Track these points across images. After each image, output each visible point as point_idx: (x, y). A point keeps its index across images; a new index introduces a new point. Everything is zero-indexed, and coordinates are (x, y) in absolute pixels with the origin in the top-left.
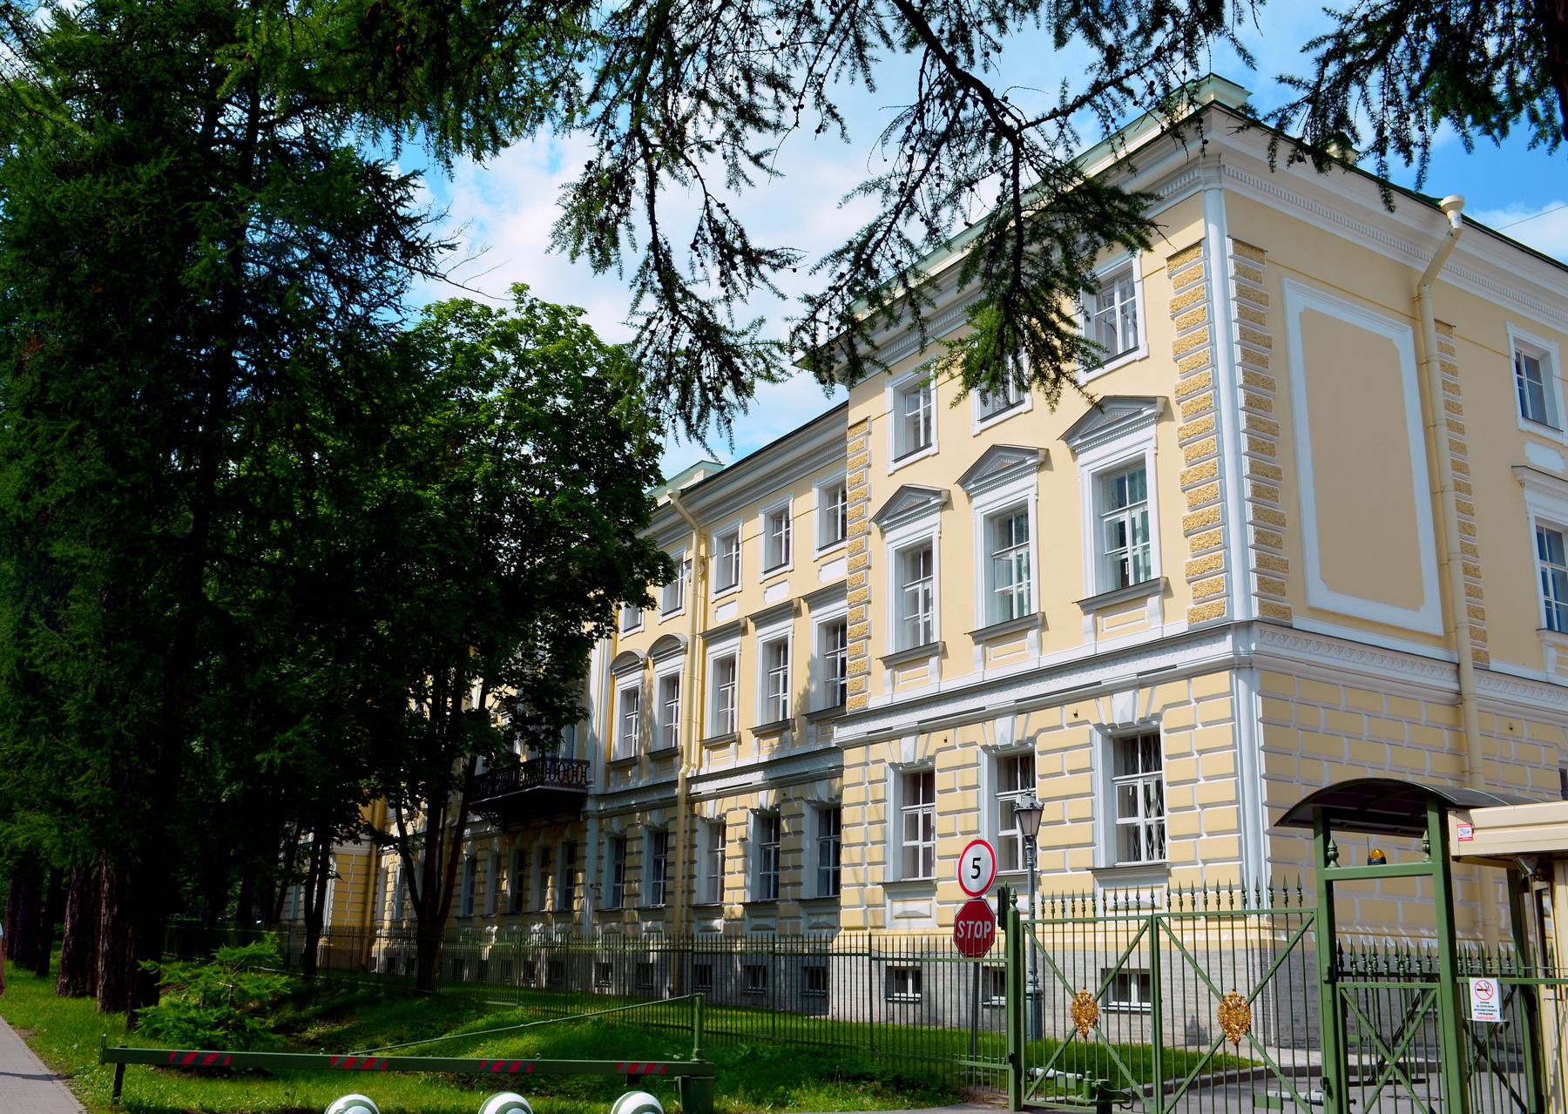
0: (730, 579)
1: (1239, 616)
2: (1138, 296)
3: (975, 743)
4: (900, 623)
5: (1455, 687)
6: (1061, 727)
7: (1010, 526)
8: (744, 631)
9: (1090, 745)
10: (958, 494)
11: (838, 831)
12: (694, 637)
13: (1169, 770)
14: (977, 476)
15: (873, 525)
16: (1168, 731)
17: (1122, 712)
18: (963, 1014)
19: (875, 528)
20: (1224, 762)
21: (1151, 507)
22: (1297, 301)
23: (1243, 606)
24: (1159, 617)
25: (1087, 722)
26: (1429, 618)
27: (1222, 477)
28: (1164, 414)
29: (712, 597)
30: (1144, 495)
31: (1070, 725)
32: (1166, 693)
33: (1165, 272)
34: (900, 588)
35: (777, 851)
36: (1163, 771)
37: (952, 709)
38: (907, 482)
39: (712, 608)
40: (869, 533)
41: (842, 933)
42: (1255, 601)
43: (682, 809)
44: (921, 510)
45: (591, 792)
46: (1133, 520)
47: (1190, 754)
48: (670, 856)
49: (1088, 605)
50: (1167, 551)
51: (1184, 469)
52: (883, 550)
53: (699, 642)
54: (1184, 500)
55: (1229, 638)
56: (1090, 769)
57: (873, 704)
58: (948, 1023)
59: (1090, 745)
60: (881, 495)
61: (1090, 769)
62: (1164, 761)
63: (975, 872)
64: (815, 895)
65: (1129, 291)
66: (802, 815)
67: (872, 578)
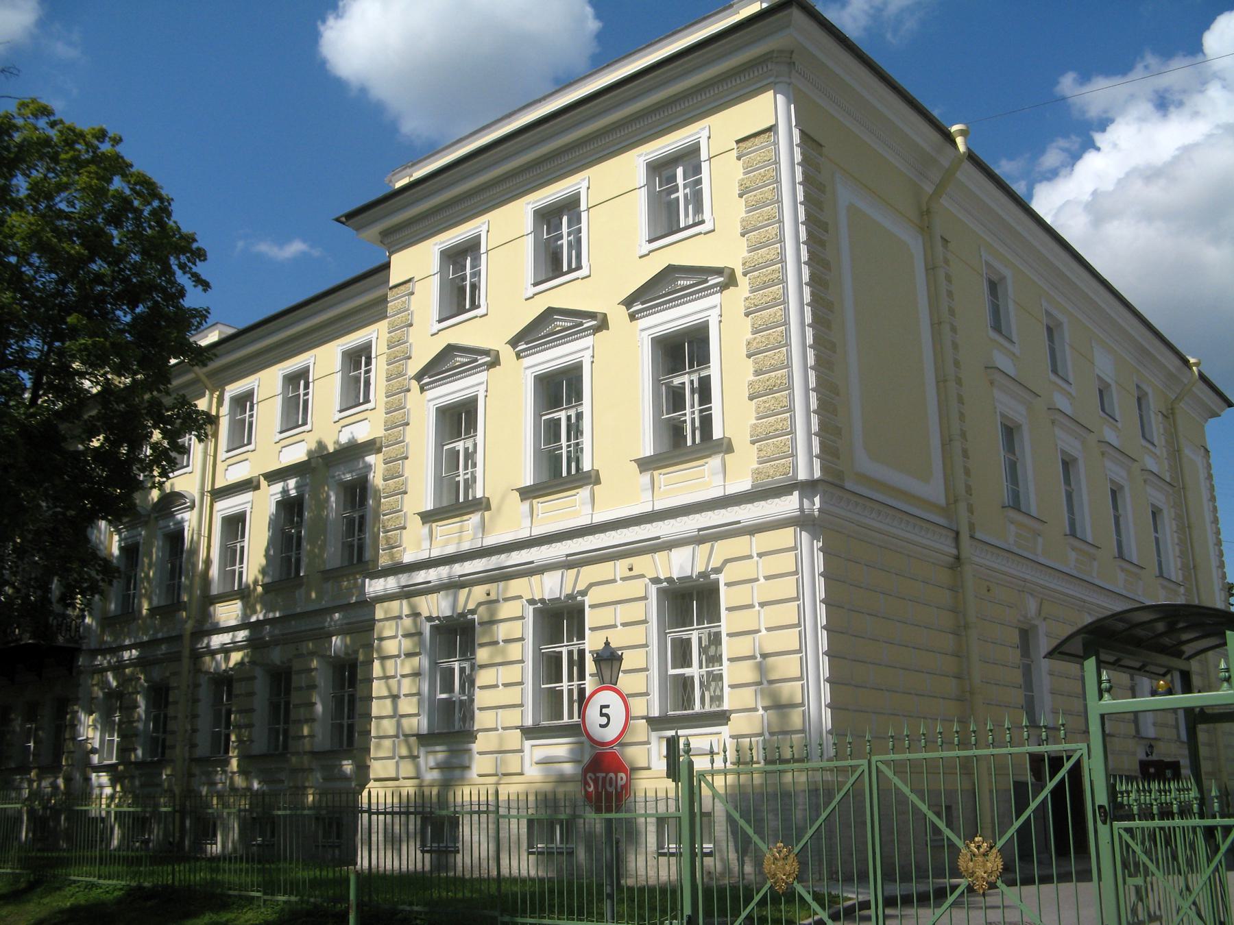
0: (242, 435)
1: (802, 475)
2: (584, 225)
3: (520, 597)
4: (439, 480)
5: (954, 551)
6: (614, 581)
7: (559, 389)
8: (257, 487)
9: (645, 598)
10: (507, 354)
11: (288, 691)
12: (202, 495)
13: (727, 623)
14: (534, 334)
15: (414, 383)
16: (591, 606)
17: (681, 567)
18: (366, 854)
19: (414, 385)
20: (788, 613)
21: (586, 408)
22: (845, 195)
23: (806, 468)
24: (721, 476)
25: (643, 576)
26: (934, 490)
27: (788, 345)
28: (729, 280)
29: (222, 454)
30: (579, 397)
31: (623, 579)
32: (724, 549)
33: (734, 153)
34: (439, 445)
35: (166, 717)
36: (586, 641)
37: (621, 540)
38: (453, 342)
39: (220, 467)
40: (409, 390)
41: (371, 784)
42: (817, 464)
43: (186, 662)
44: (471, 369)
45: (84, 647)
46: (692, 382)
47: (751, 606)
48: (171, 711)
49: (645, 464)
50: (733, 412)
51: (750, 336)
52: (424, 408)
53: (207, 499)
54: (749, 366)
55: (796, 493)
56: (645, 622)
57: (408, 558)
58: (459, 868)
59: (645, 598)
60: (424, 349)
61: (645, 622)
62: (587, 632)
63: (604, 720)
64: (327, 747)
65: (576, 219)
66: (253, 678)
67: (410, 434)
